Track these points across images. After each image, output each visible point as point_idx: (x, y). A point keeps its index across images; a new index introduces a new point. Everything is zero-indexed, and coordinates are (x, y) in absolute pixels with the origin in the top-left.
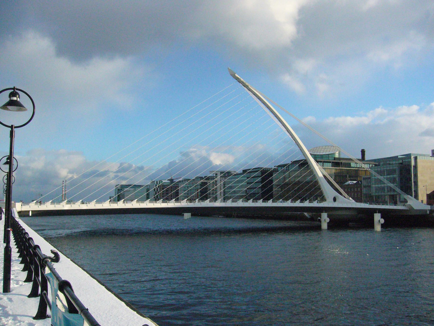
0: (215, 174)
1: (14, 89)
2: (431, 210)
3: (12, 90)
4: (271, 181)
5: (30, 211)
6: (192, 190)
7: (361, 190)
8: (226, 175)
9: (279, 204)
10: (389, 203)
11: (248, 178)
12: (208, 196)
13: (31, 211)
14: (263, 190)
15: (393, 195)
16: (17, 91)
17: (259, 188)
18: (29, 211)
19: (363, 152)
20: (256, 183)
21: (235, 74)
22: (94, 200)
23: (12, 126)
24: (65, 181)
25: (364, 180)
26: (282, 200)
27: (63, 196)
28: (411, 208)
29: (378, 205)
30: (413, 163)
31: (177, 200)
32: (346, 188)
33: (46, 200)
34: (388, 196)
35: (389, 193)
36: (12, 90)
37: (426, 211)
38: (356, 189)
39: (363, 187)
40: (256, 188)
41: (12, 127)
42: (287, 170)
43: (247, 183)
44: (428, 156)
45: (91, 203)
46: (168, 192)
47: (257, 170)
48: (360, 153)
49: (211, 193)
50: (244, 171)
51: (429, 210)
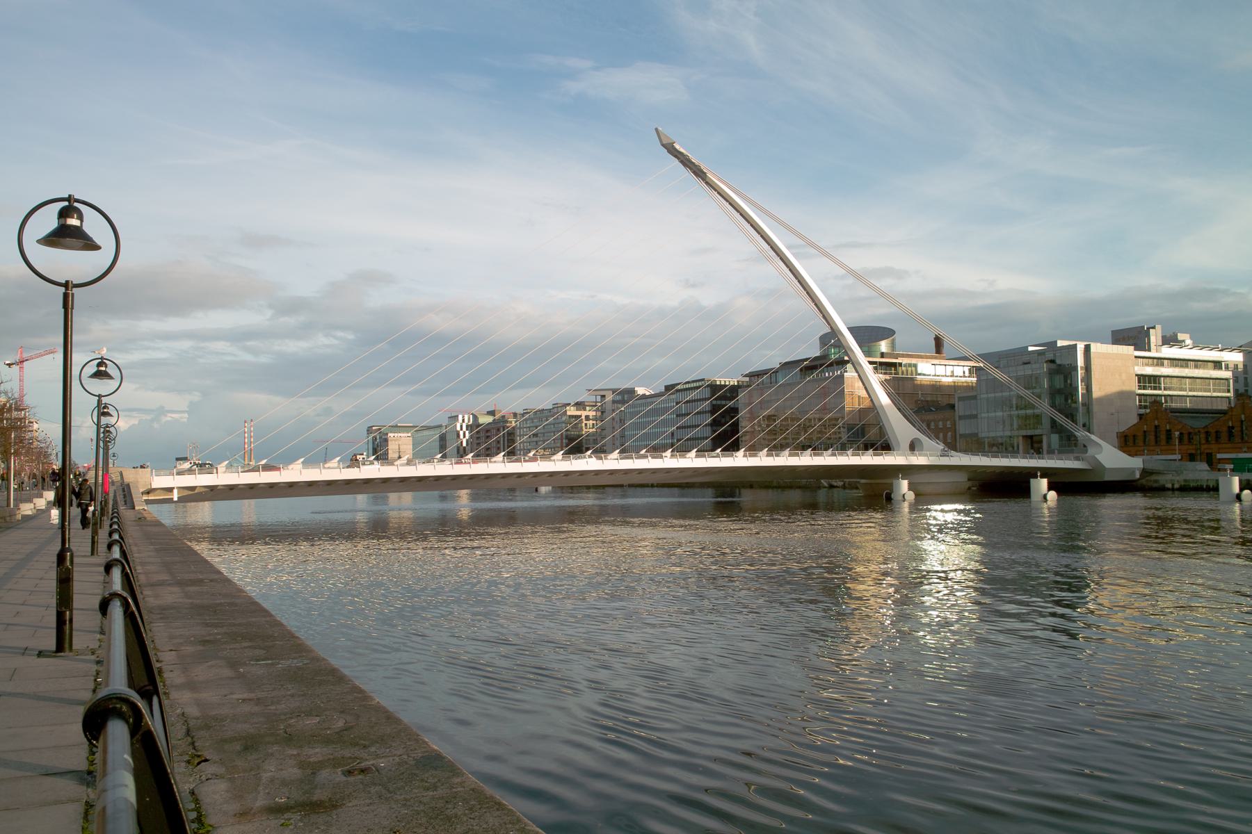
0: (600, 397)
1: (69, 199)
2: (1144, 469)
3: (66, 203)
4: (735, 411)
5: (174, 488)
6: (546, 435)
7: (954, 424)
8: (626, 399)
9: (763, 460)
10: (1024, 453)
11: (677, 403)
12: (740, 439)
13: (177, 488)
14: (715, 431)
15: (1031, 437)
16: (76, 204)
17: (706, 425)
18: (170, 490)
19: (495, 405)
20: (698, 413)
21: (674, 143)
22: (298, 459)
23: (67, 282)
24: (249, 420)
25: (960, 403)
26: (646, 452)
27: (246, 456)
28: (1099, 467)
29: (1030, 460)
30: (1080, 362)
31: (511, 454)
32: (939, 420)
33: (289, 460)
34: (1021, 438)
35: (1024, 433)
36: (66, 203)
37: (1132, 471)
38: (941, 423)
39: (957, 419)
40: (699, 426)
41: (66, 285)
42: (772, 382)
43: (677, 416)
44: (79, 529)
45: (290, 467)
46: (489, 434)
47: (698, 384)
48: (933, 343)
49: (591, 440)
50: (668, 388)
51: (1138, 469)
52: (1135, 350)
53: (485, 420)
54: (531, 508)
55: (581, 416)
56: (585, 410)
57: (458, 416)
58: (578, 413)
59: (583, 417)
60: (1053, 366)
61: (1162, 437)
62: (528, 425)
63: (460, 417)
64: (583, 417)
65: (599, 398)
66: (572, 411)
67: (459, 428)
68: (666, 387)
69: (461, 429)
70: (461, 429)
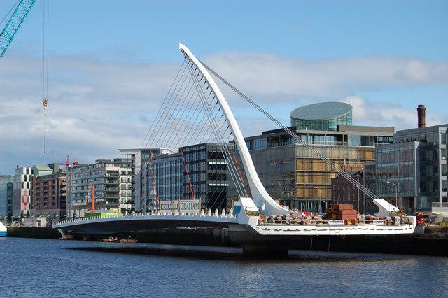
19: (421, 110)
52: (442, 134)
53: (44, 172)
54: (188, 251)
55: (118, 172)
56: (122, 167)
57: (22, 168)
58: (116, 169)
59: (120, 173)
60: (424, 144)
61: (155, 231)
62: (77, 179)
63: (25, 169)
64: (120, 173)
65: (130, 157)
66: (110, 168)
67: (23, 180)
68: (263, 133)
69: (25, 180)
70: (25, 180)
